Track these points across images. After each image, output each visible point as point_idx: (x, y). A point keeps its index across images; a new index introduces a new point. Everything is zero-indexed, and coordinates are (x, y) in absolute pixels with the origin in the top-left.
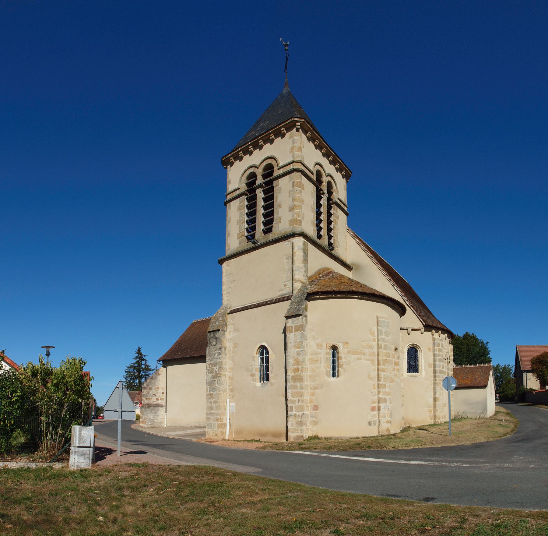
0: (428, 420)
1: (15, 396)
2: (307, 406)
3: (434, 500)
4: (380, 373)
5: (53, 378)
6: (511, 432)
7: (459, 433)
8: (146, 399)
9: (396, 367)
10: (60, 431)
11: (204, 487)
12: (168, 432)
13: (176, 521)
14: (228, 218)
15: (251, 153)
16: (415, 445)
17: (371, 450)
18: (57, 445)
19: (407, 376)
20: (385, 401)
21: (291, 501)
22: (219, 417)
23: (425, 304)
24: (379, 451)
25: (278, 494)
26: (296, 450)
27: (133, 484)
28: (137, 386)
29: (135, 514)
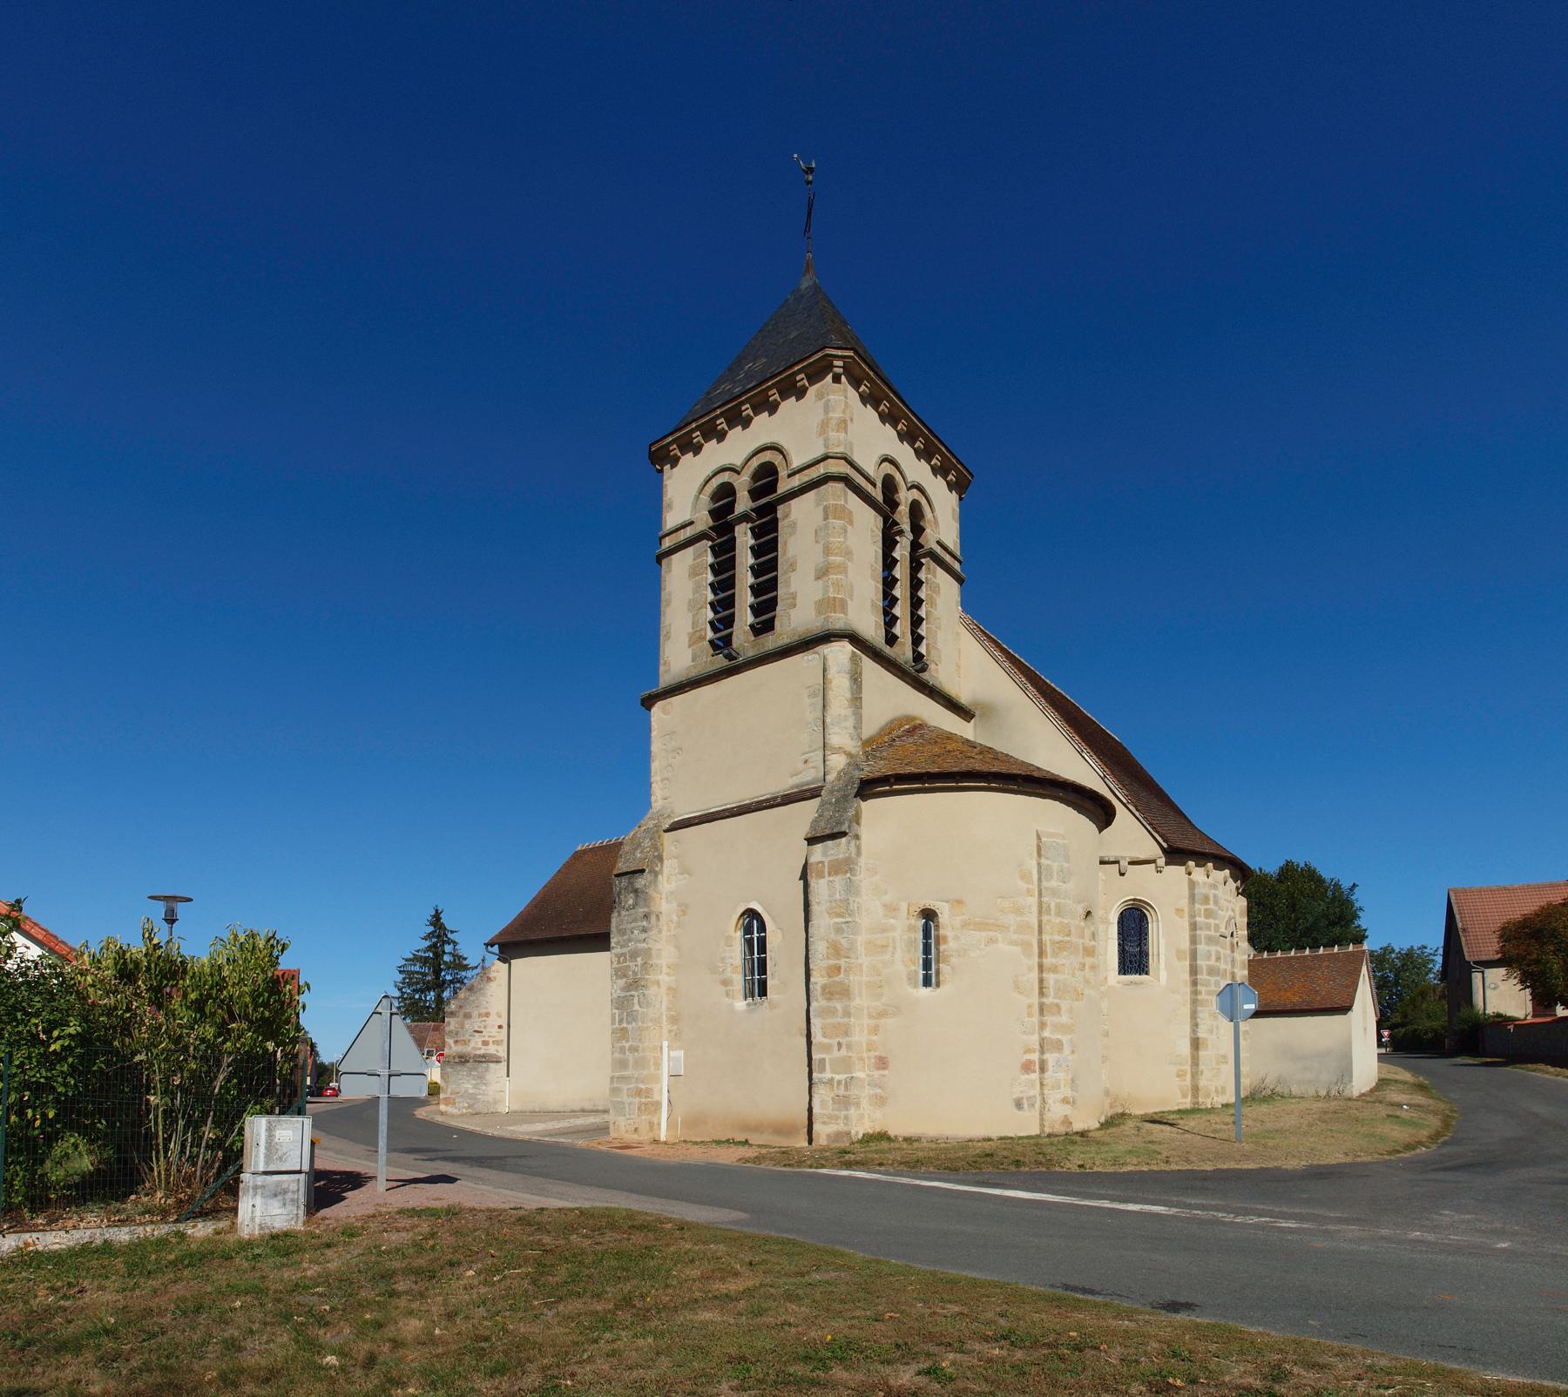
0: (1173, 1097)
1: (59, 1038)
2: (862, 1059)
3: (1194, 1310)
4: (1044, 975)
5: (188, 986)
6: (1430, 1141)
7: (1267, 1134)
8: (456, 1042)
9: (1089, 961)
10: (209, 1132)
11: (605, 1262)
12: (515, 1124)
13: (533, 1349)
14: (664, 596)
15: (721, 437)
16: (1139, 1163)
17: (1020, 1172)
18: (198, 1174)
19: (1119, 982)
20: (1058, 1046)
21: (821, 1293)
22: (642, 1086)
23: (1167, 792)
24: (1041, 1173)
25: (786, 1274)
26: (833, 1167)
27: (421, 1262)
28: (432, 1009)
29: (427, 1340)
